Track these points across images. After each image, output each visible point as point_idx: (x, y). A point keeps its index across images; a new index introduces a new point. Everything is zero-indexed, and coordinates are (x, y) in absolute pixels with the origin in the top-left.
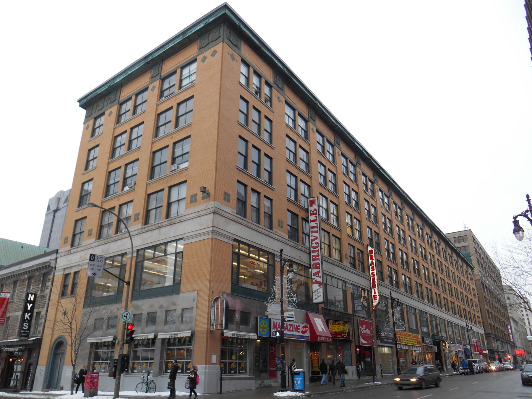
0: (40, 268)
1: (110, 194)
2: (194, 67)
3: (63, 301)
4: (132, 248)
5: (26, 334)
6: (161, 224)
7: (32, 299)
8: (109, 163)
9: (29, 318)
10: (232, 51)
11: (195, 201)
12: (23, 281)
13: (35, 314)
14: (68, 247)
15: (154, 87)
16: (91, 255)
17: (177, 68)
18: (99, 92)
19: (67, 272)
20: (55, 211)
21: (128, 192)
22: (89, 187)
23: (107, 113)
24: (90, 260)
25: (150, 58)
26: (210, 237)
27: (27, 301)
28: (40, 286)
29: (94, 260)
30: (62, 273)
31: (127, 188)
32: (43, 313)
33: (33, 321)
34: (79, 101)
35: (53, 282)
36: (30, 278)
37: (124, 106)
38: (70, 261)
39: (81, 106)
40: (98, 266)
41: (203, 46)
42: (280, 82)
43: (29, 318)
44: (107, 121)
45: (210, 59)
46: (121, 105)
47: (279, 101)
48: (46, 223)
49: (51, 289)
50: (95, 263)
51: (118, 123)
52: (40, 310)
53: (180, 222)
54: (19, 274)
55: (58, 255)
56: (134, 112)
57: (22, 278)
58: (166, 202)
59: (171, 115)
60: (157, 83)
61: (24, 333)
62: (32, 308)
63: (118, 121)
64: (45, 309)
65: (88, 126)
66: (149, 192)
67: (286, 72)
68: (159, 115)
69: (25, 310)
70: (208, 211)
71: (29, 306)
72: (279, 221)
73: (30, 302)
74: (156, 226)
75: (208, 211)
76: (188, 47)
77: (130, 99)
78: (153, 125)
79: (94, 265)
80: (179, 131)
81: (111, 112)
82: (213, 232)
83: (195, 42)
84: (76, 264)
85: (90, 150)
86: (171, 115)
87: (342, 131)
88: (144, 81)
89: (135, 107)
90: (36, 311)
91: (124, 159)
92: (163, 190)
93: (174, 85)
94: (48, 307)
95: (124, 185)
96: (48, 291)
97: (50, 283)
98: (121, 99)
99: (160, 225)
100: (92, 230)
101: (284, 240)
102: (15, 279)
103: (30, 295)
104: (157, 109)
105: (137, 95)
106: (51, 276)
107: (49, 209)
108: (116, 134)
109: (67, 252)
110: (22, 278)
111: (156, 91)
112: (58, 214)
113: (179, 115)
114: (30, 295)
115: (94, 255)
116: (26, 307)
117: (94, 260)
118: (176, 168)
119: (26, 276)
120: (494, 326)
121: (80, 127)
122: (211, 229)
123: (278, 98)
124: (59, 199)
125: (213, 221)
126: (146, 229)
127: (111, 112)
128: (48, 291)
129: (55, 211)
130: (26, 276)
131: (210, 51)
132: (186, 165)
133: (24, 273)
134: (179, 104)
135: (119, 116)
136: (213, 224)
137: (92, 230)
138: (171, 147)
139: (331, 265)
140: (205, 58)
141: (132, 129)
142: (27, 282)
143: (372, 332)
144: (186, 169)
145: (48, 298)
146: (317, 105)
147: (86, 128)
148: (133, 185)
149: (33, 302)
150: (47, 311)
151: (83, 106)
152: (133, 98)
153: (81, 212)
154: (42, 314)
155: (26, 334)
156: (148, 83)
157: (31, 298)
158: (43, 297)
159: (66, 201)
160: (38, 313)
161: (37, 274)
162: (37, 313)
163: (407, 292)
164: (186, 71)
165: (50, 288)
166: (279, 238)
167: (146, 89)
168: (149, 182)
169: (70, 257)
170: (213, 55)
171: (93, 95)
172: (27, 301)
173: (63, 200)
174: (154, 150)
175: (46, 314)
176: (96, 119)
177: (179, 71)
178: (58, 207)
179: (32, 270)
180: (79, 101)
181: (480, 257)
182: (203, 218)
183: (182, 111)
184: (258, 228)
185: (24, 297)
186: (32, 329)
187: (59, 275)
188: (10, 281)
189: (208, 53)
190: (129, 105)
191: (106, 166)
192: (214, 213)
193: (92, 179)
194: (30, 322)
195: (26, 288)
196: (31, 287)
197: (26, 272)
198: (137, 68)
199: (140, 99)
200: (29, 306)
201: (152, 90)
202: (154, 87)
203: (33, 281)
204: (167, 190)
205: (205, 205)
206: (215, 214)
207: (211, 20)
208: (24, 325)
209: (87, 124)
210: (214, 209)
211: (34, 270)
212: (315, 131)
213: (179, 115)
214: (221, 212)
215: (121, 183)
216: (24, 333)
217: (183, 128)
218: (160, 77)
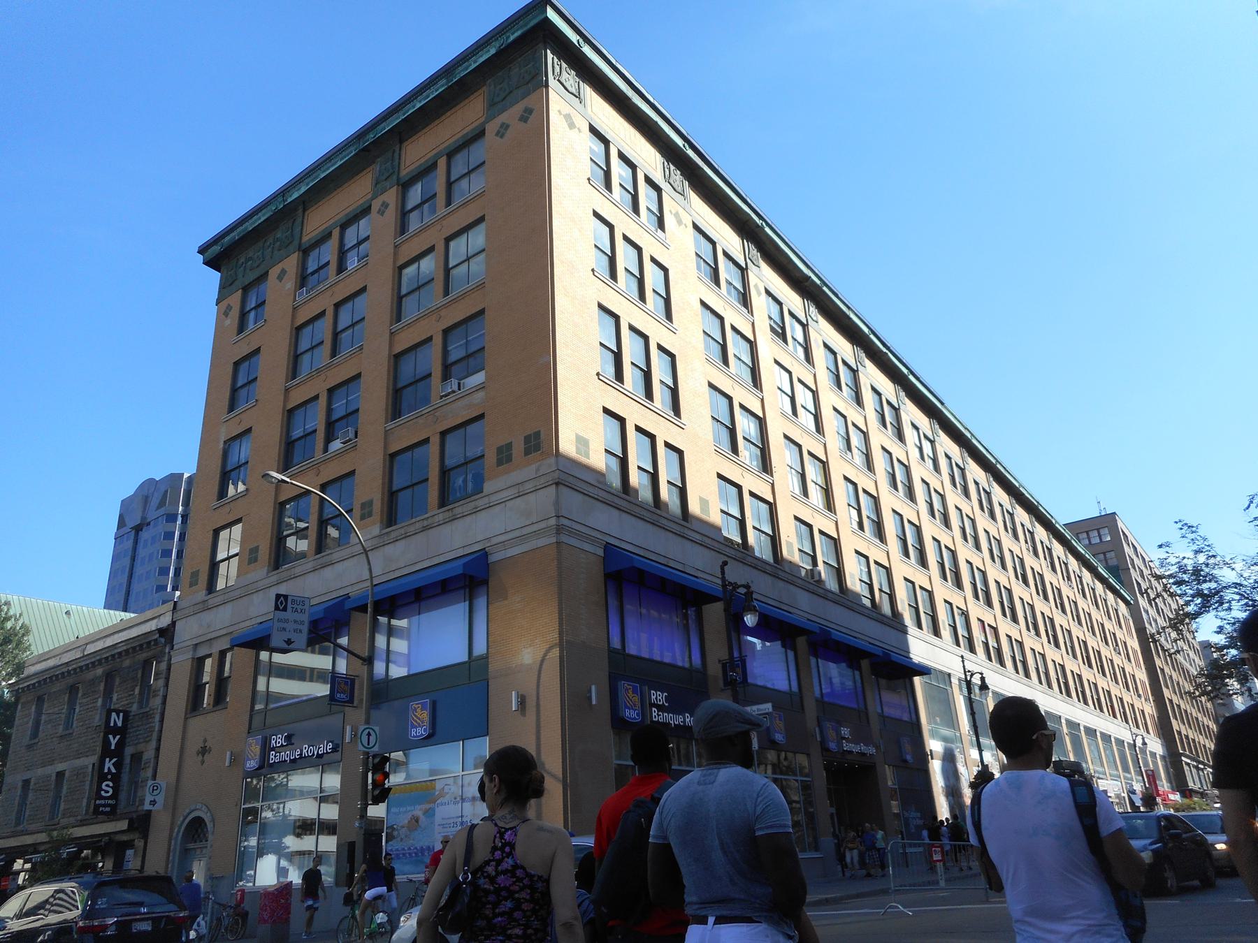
0: (134, 648)
1: (295, 461)
3: (196, 723)
4: (372, 578)
5: (108, 809)
6: (430, 521)
7: (120, 724)
8: (287, 390)
9: (114, 771)
10: (567, 109)
11: (509, 459)
12: (93, 682)
13: (127, 760)
14: (201, 594)
15: (385, 205)
16: (278, 596)
17: (439, 155)
18: (249, 226)
19: (202, 652)
20: (138, 529)
21: (340, 454)
22: (244, 451)
23: (274, 273)
24: (277, 608)
25: (371, 137)
26: (554, 540)
27: (110, 730)
28: (137, 691)
29: (285, 609)
30: (190, 655)
31: (336, 445)
32: (149, 754)
33: (125, 778)
34: (202, 251)
35: (167, 679)
36: (109, 677)
37: (314, 254)
38: (209, 626)
39: (208, 263)
40: (295, 622)
41: (497, 100)
42: (677, 176)
43: (114, 771)
44: (280, 288)
46: (305, 252)
47: (680, 222)
48: (115, 558)
49: (165, 697)
50: (288, 615)
51: (403, 232)
52: (141, 747)
53: (476, 511)
54: (81, 667)
55: (178, 615)
56: (341, 268)
57: (90, 675)
58: (437, 469)
59: (324, 329)
60: (391, 196)
61: (104, 806)
62: (121, 744)
63: (403, 228)
64: (154, 744)
65: (229, 308)
66: (393, 449)
67: (690, 153)
68: (299, 329)
69: (106, 752)
70: (542, 480)
71: (114, 741)
72: (701, 499)
73: (115, 731)
74: (418, 526)
75: (542, 480)
76: (472, 97)
77: (326, 236)
78: (390, 292)
79: (287, 621)
80: (455, 301)
81: (283, 272)
82: (559, 529)
83: (476, 94)
84: (224, 632)
85: (237, 364)
86: (324, 329)
87: (820, 288)
88: (358, 191)
89: (342, 254)
90: (129, 751)
91: (323, 377)
92: (426, 441)
93: (328, 263)
94: (159, 740)
95: (329, 439)
96: (156, 702)
97: (161, 682)
98: (305, 239)
99: (425, 523)
100: (257, 548)
101: (716, 545)
102: (70, 680)
103: (114, 715)
104: (395, 254)
105: (344, 226)
106: (163, 666)
107: (121, 523)
108: (299, 322)
109: (201, 606)
110: (90, 675)
111: (391, 214)
112: (145, 535)
113: (340, 328)
114: (114, 715)
115: (286, 597)
116: (106, 743)
117: (285, 609)
118: (455, 387)
119: (99, 671)
120: (1187, 737)
121: (210, 312)
122: (553, 522)
123: (677, 215)
124: (146, 500)
125: (557, 503)
126: (393, 535)
127: (283, 272)
128: (156, 702)
129: (138, 529)
130: (99, 671)
131: (517, 109)
132: (479, 378)
133: (93, 663)
134: (448, 240)
135: (404, 215)
136: (557, 510)
137: (257, 548)
138: (438, 340)
139: (821, 600)
140: (505, 127)
141: (337, 306)
142: (102, 685)
143: (877, 748)
144: (481, 387)
145: (157, 718)
146: (763, 228)
147: (224, 313)
148: (351, 435)
149: (122, 731)
150: (158, 749)
151: (212, 263)
152: (336, 233)
153: (227, 509)
154: (145, 757)
155: (108, 809)
156: (369, 196)
157: (117, 720)
158: (147, 716)
159: (162, 504)
160: (137, 757)
161: (127, 663)
162: (132, 756)
163: (990, 659)
165: (161, 693)
166: (705, 539)
167: (365, 211)
168: (391, 425)
169: (207, 617)
170: (524, 119)
171: (235, 235)
172: (110, 730)
173: (155, 502)
174: (398, 349)
175: (157, 757)
176: (246, 290)
177: (442, 163)
178: (143, 518)
179: (113, 656)
180: (202, 251)
181: (1142, 576)
182: (532, 497)
183: (344, 320)
184: (655, 517)
185: (97, 719)
186: (123, 796)
187: (181, 660)
188: (56, 687)
189: (511, 115)
190: (328, 252)
191: (282, 398)
192: (557, 484)
193: (249, 430)
194: (116, 779)
195: (100, 701)
196: (115, 697)
197: (100, 661)
198: (340, 163)
199: (351, 237)
200: (114, 741)
201: (381, 212)
202: (385, 205)
203: (117, 681)
204: (435, 440)
205: (534, 467)
206: (561, 487)
207: (512, 38)
208: (104, 787)
209: (225, 303)
210: (556, 475)
211: (120, 653)
212: (763, 291)
213: (340, 328)
214: (570, 479)
215: (321, 435)
216: (104, 806)
217: (464, 296)
218: (398, 179)
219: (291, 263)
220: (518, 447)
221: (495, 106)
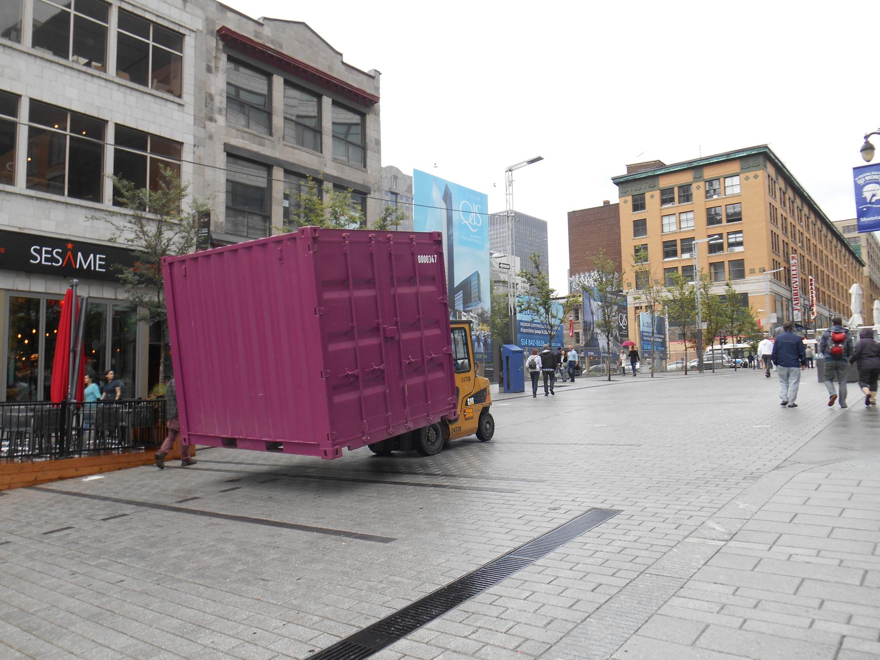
2: (736, 180)
45: (752, 180)
88: (735, 167)
140: (747, 178)
151: (617, 184)
164: (728, 182)
177: (722, 179)
180: (613, 179)
219: (657, 194)
220: (757, 270)
221: (744, 169)
